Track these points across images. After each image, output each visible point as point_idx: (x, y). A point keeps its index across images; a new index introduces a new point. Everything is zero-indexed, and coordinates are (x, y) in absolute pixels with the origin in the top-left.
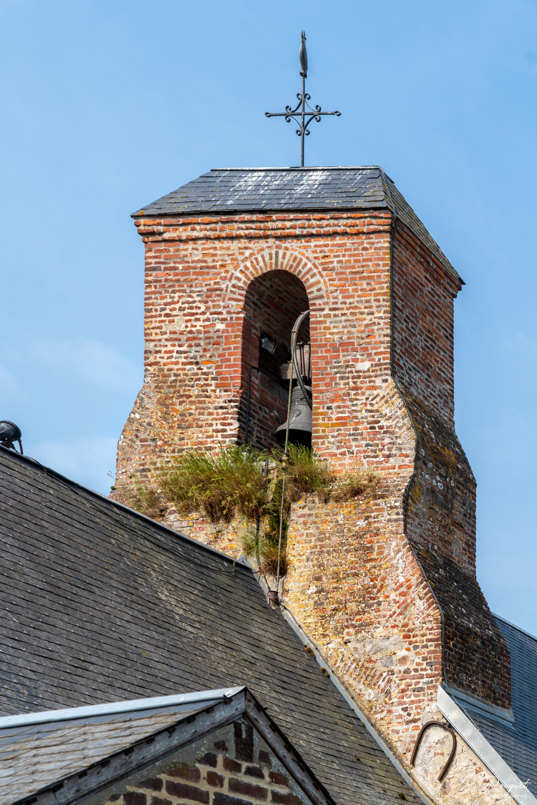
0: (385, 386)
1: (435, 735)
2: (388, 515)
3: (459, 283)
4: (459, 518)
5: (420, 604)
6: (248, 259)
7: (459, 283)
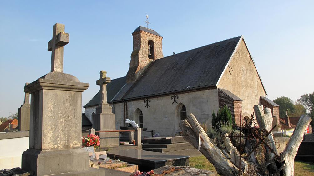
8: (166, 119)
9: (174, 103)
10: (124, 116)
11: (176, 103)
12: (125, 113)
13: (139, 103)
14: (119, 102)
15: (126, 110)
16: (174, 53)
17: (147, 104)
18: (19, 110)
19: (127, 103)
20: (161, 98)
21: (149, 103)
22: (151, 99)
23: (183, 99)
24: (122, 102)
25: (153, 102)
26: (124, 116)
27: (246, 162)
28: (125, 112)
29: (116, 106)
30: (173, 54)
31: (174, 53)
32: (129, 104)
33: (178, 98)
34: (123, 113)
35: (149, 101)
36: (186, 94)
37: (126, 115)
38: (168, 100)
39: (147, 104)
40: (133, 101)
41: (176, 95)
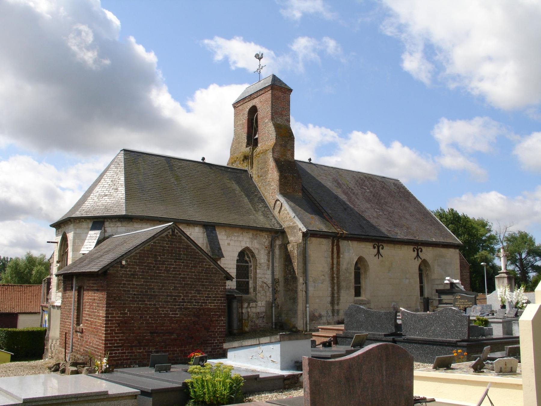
0: (271, 124)
1: (278, 202)
2: (270, 155)
3: (290, 90)
4: (289, 148)
5: (275, 172)
6: (250, 105)
7: (290, 90)
8: (407, 281)
9: (377, 256)
10: (332, 268)
11: (419, 259)
12: (333, 262)
13: (363, 246)
14: (321, 235)
15: (335, 256)
16: (203, 159)
17: (418, 254)
18: (433, 400)
19: (338, 242)
20: (399, 246)
21: (381, 251)
22: (384, 245)
23: (428, 253)
24: (328, 238)
25: (387, 251)
26: (332, 268)
27: (34, 272)
28: (332, 258)
29: (311, 243)
30: (307, 161)
31: (203, 159)
32: (343, 244)
33: (421, 251)
34: (330, 260)
35: (420, 250)
36: (431, 248)
37: (335, 266)
38: (408, 252)
39: (418, 254)
40: (351, 240)
41: (419, 247)
